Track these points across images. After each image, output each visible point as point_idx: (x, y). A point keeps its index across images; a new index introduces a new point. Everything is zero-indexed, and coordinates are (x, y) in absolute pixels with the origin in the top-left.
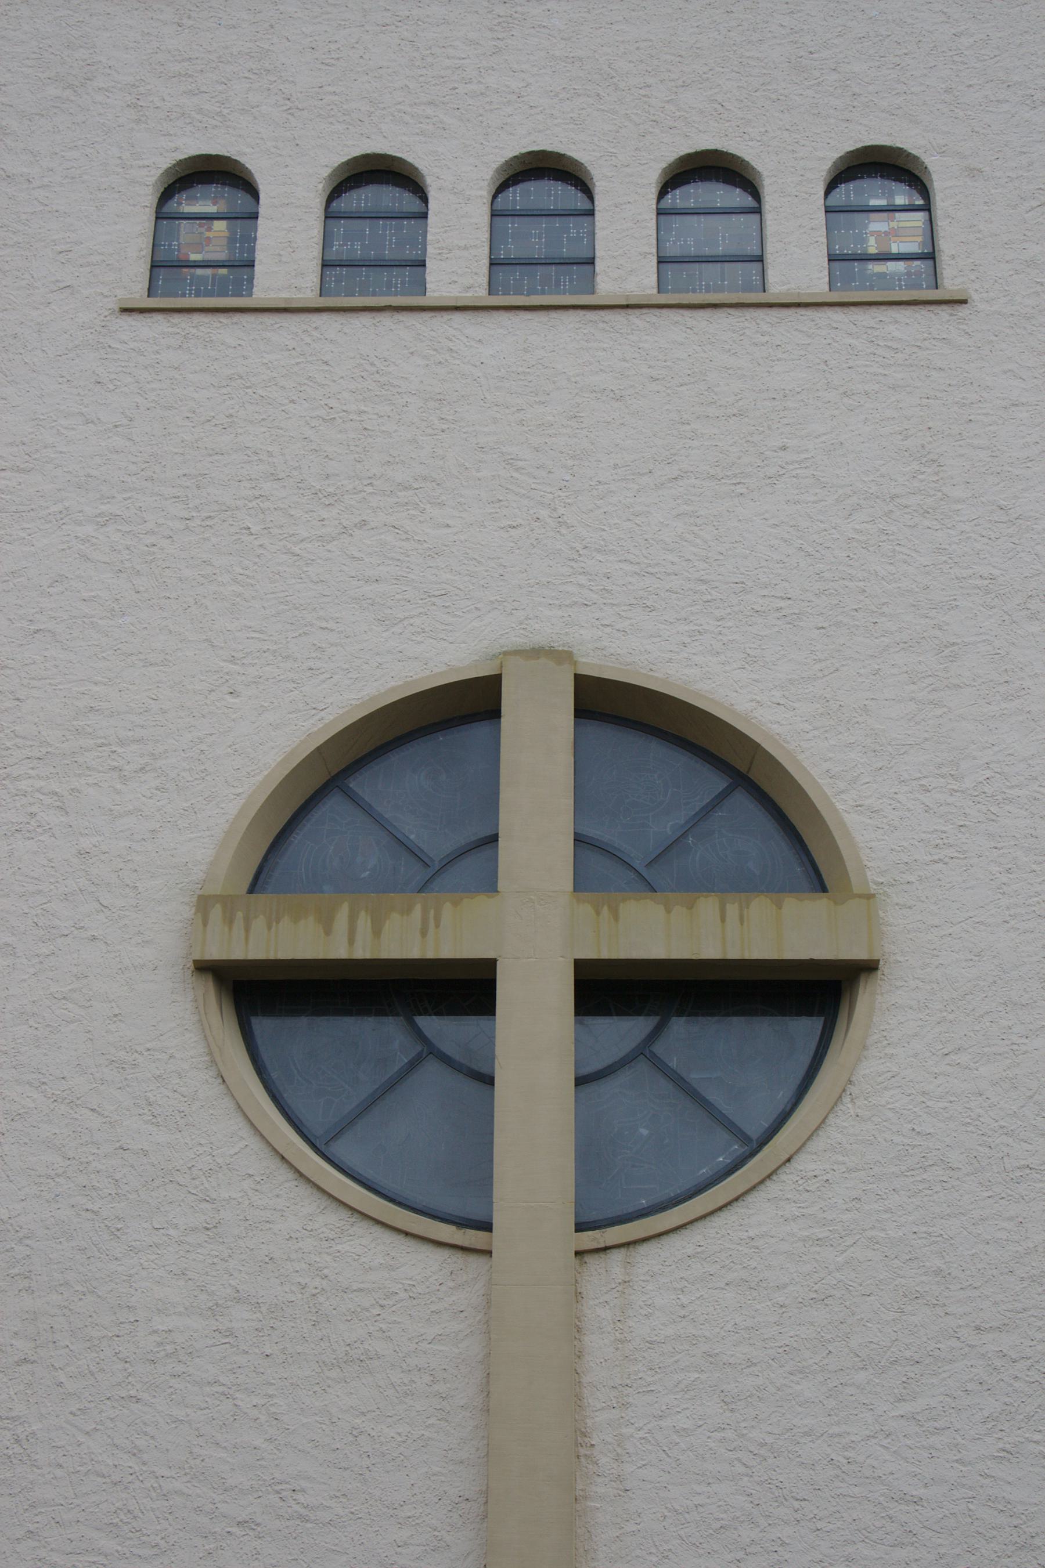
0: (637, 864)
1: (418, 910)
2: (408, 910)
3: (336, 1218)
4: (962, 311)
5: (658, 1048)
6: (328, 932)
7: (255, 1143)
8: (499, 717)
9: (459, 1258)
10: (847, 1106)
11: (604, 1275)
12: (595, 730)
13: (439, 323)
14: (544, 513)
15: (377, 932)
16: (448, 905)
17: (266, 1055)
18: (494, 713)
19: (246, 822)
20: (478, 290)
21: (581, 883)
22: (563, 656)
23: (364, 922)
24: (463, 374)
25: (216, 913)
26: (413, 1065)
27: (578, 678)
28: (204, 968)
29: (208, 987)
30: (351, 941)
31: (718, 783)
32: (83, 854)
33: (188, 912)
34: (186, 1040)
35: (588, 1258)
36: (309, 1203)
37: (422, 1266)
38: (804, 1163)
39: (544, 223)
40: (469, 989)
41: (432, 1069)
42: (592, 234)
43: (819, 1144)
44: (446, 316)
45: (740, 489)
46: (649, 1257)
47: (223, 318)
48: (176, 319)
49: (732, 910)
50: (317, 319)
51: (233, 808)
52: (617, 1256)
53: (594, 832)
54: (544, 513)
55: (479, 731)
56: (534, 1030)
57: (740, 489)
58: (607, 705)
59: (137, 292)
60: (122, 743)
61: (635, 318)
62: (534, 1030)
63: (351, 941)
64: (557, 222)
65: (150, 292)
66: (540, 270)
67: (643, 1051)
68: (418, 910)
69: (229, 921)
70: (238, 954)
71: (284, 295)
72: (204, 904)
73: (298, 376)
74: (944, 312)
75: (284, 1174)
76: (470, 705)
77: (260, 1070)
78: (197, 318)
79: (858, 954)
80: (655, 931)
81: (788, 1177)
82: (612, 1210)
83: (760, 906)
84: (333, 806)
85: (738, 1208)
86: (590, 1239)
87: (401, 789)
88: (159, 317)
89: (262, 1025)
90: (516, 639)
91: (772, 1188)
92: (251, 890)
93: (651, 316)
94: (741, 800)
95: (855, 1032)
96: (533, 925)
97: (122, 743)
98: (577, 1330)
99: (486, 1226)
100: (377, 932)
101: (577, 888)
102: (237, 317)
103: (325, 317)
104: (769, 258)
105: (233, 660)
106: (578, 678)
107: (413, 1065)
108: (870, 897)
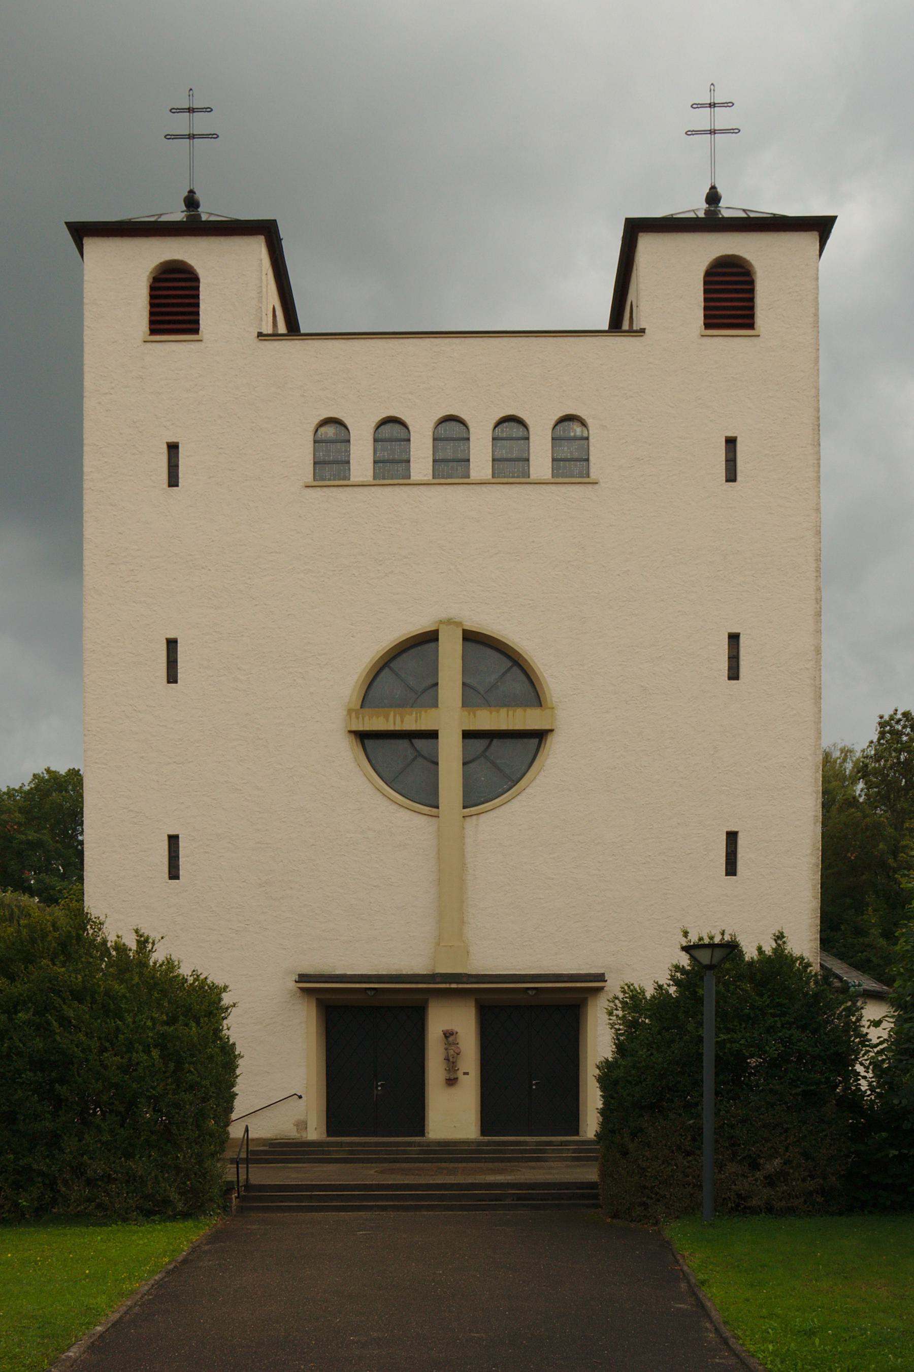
0: (482, 692)
1: (414, 715)
2: (411, 714)
3: (395, 807)
4: (596, 487)
5: (487, 754)
6: (387, 720)
7: (370, 785)
8: (437, 738)
9: (430, 818)
10: (542, 773)
11: (471, 823)
12: (468, 644)
13: (415, 489)
14: (452, 567)
15: (402, 722)
16: (423, 713)
17: (368, 750)
18: (437, 640)
19: (360, 683)
20: (429, 477)
21: (465, 704)
22: (458, 624)
23: (398, 718)
24: (424, 505)
25: (353, 715)
26: (414, 759)
27: (464, 630)
28: (350, 732)
29: (353, 736)
30: (395, 724)
31: (510, 664)
32: (311, 693)
33: (345, 713)
34: (347, 758)
35: (467, 819)
36: (387, 803)
37: (419, 821)
38: (529, 790)
39: (452, 443)
40: (433, 735)
41: (420, 760)
42: (469, 448)
43: (533, 784)
44: (418, 487)
45: (518, 558)
46: (483, 818)
47: (341, 489)
48: (325, 489)
49: (511, 713)
50: (374, 489)
51: (356, 677)
52: (474, 817)
53: (468, 681)
54: (452, 567)
55: (432, 645)
56: (450, 753)
57: (518, 558)
58: (472, 638)
59: (309, 478)
60: (319, 654)
61: (484, 488)
62: (450, 753)
63: (395, 724)
64: (456, 443)
65: (315, 479)
66: (451, 464)
67: (483, 754)
68: (414, 715)
69: (358, 718)
70: (361, 729)
71: (361, 479)
72: (350, 711)
73: (365, 509)
74: (590, 487)
75: (379, 794)
76: (430, 638)
77: (369, 761)
78: (332, 489)
79: (548, 727)
80: (488, 720)
81: (524, 794)
82: (475, 797)
83: (519, 711)
84: (386, 670)
85: (509, 804)
86: (467, 811)
87: (408, 662)
88: (319, 489)
89: (366, 741)
90: (444, 615)
91: (519, 797)
92: (361, 707)
93: (489, 487)
94: (515, 668)
95: (546, 751)
96: (449, 717)
97: (319, 654)
98: (463, 837)
99: (437, 807)
100: (402, 722)
101: (463, 706)
102: (346, 488)
103: (376, 488)
104: (531, 459)
105: (352, 624)
106: (464, 630)
107: (414, 759)
108: (553, 708)
